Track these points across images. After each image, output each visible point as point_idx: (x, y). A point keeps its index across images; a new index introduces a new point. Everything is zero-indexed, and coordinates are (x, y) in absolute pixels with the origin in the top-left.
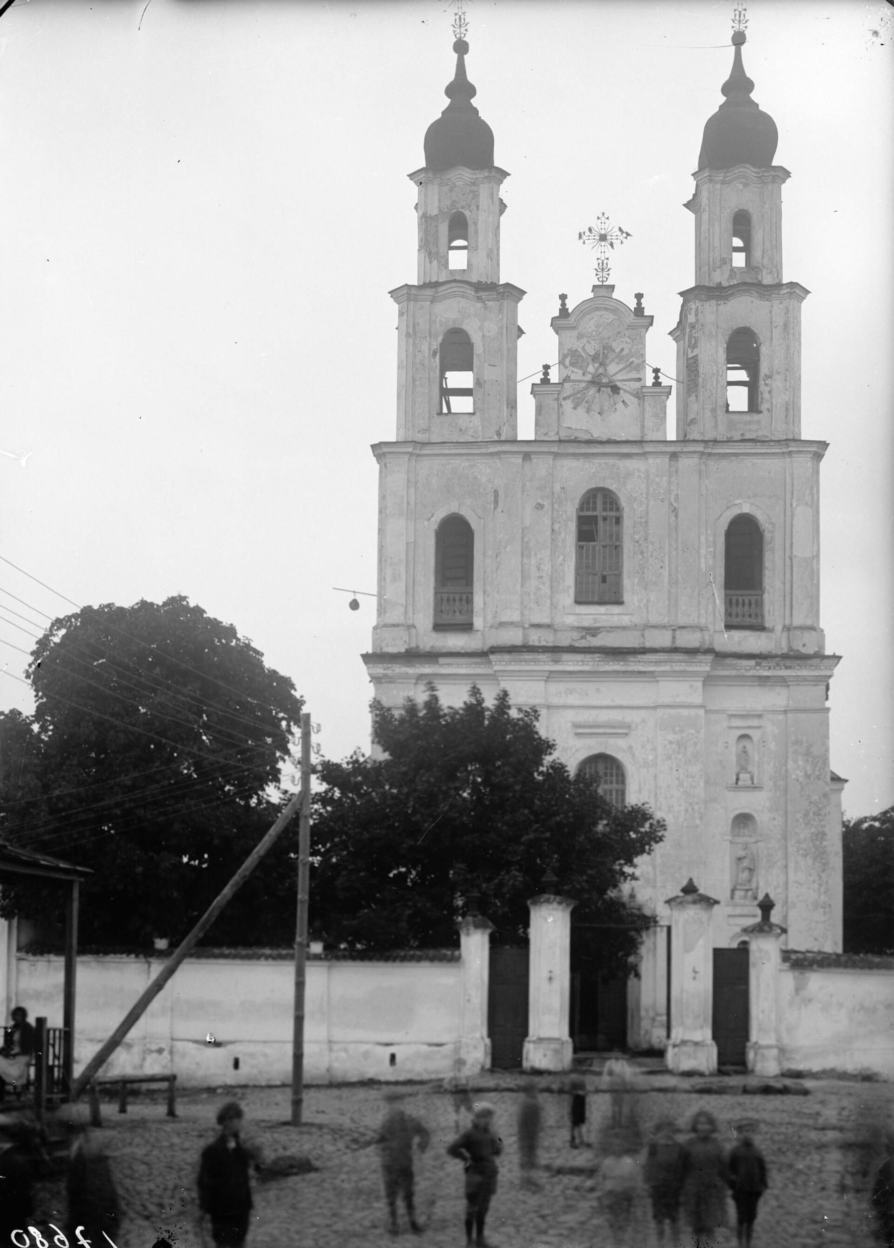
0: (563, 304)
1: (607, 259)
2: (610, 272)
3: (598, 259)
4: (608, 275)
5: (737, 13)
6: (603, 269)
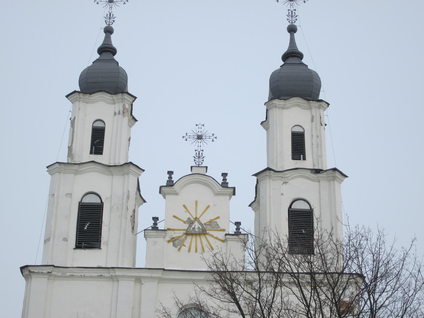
0: (170, 178)
1: (202, 151)
2: (204, 159)
3: (196, 150)
4: (203, 160)
5: (290, 12)
6: (199, 157)
